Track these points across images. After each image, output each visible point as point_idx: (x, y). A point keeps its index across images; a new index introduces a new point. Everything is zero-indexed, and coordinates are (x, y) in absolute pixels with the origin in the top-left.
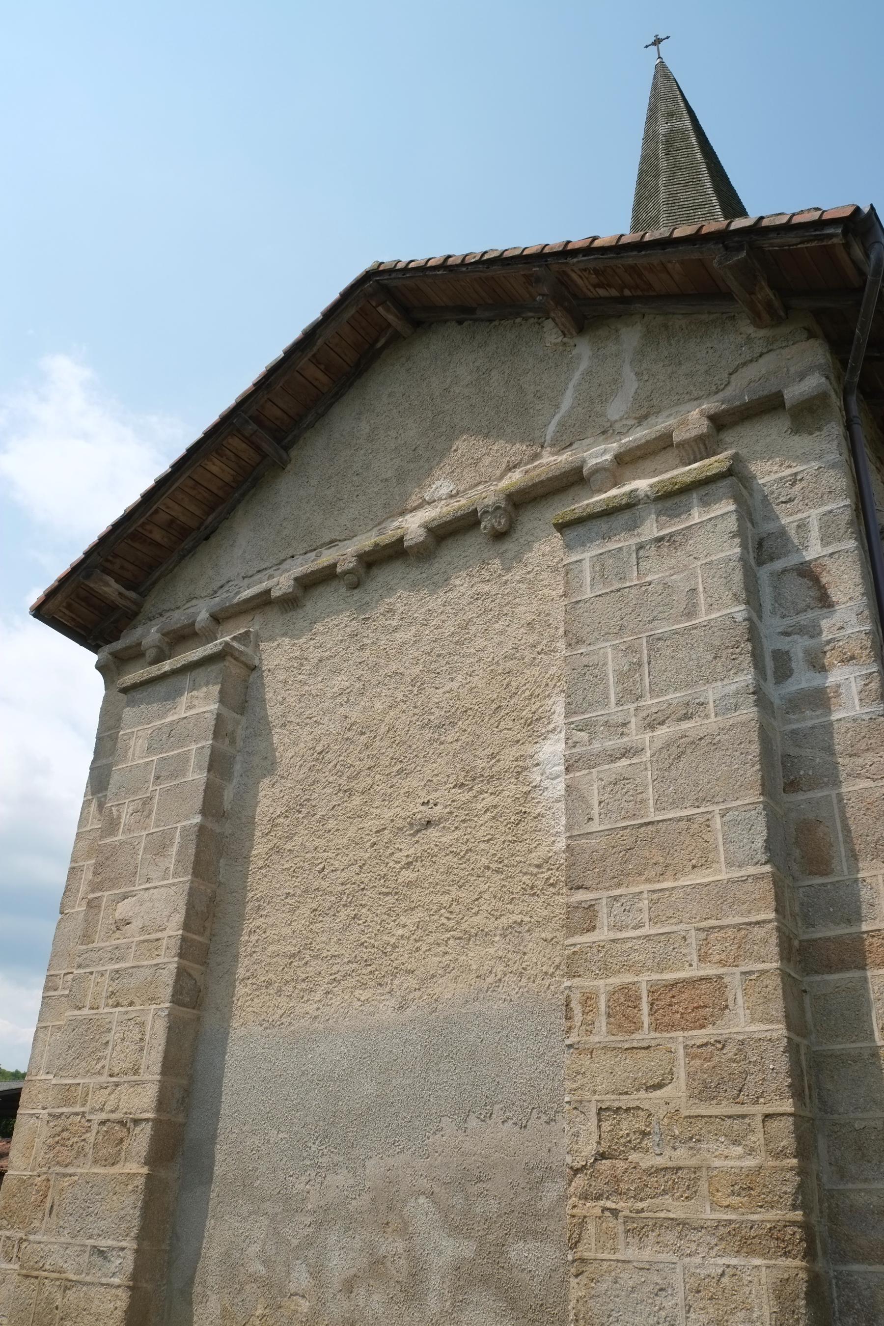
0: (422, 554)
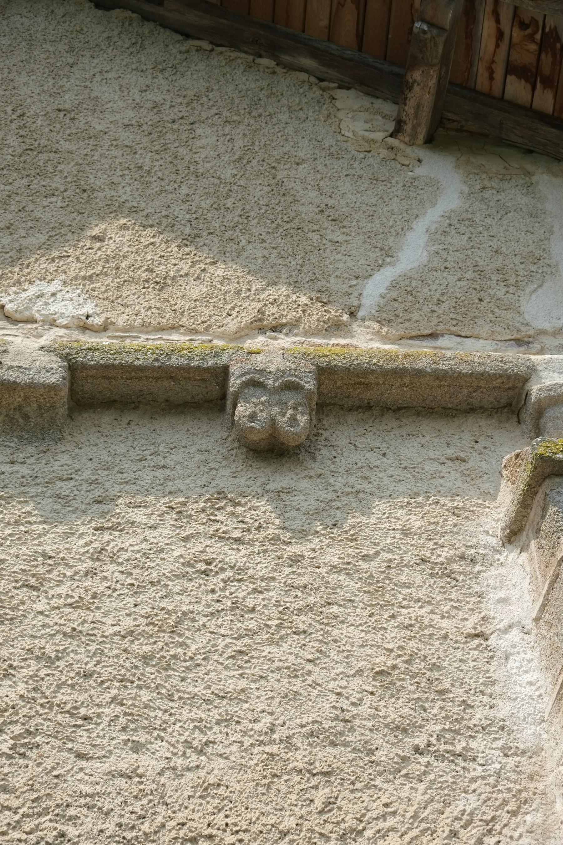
0: (26, 417)
